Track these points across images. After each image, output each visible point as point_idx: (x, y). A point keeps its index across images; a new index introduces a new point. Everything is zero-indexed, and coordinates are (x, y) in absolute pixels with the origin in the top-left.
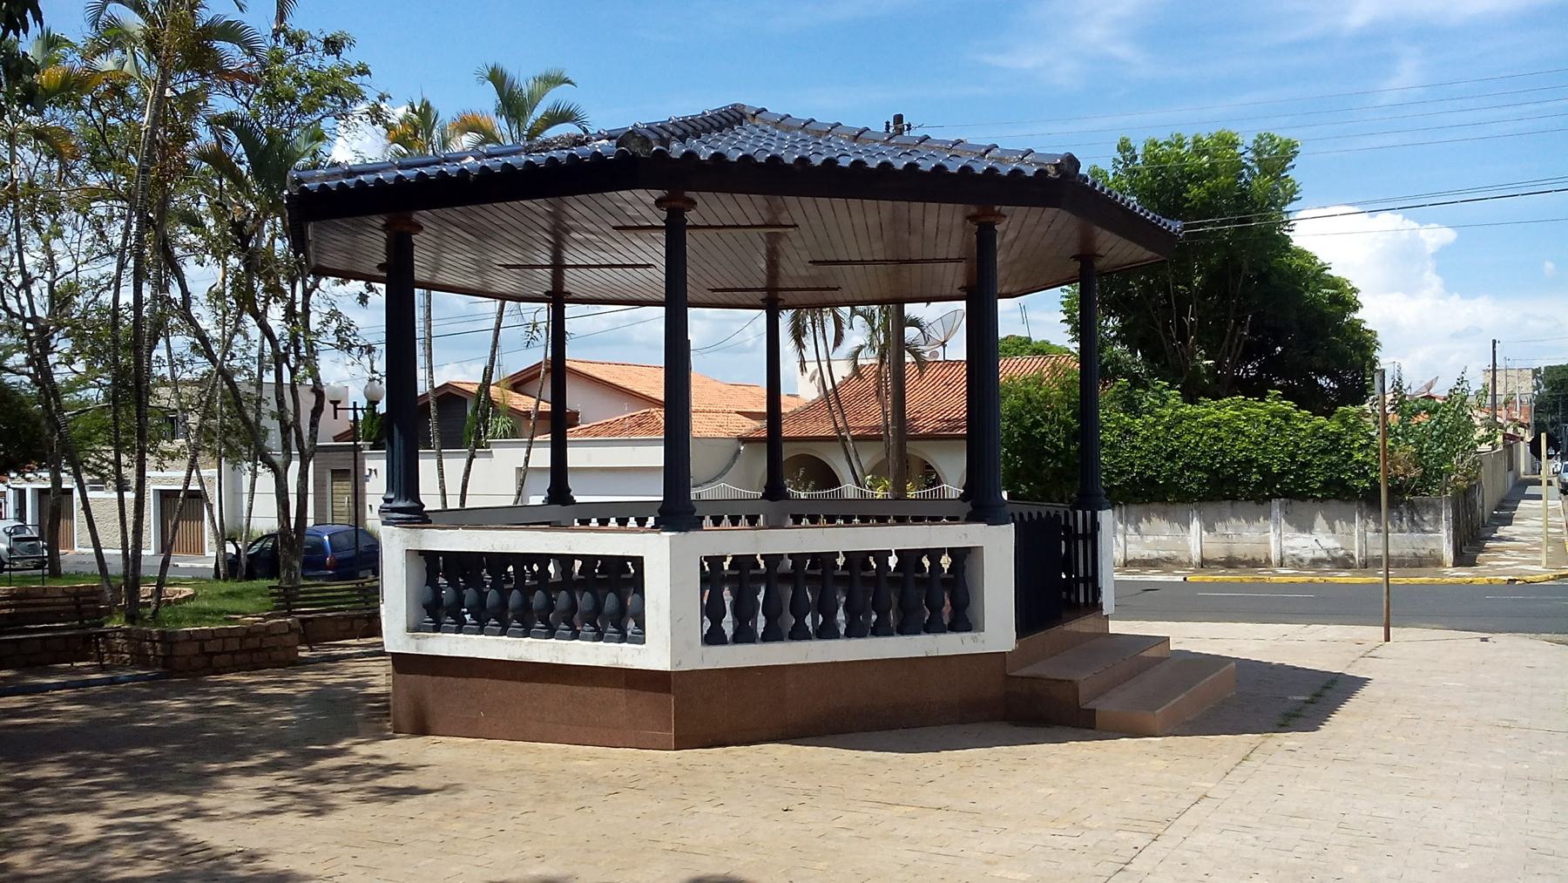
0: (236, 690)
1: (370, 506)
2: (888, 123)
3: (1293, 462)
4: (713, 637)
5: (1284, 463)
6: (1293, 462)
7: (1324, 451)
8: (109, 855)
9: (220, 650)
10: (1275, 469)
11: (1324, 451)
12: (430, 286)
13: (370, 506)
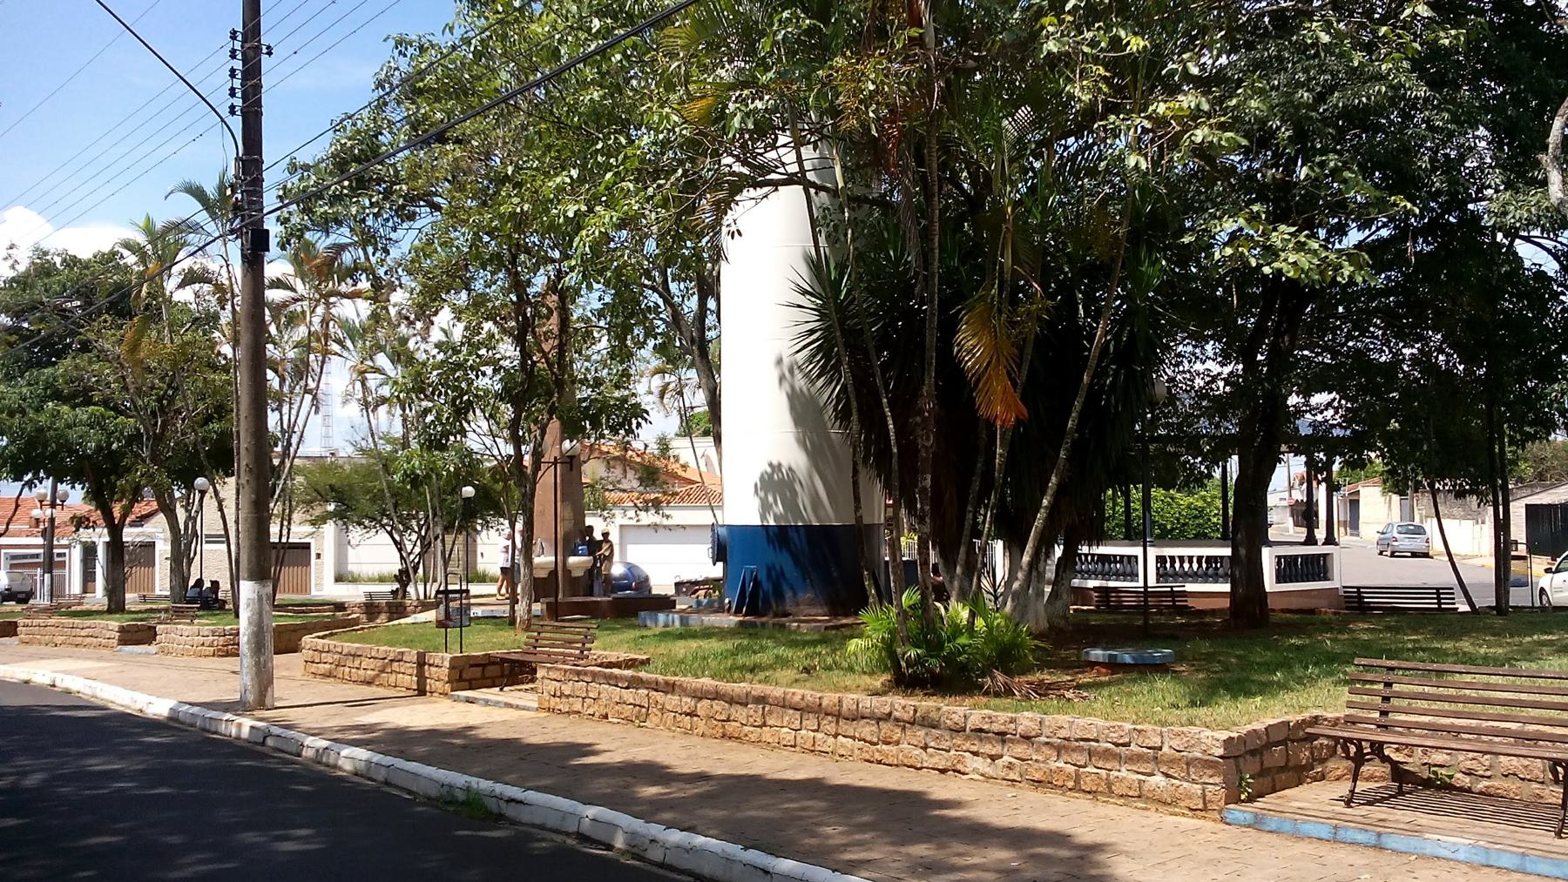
0: (105, 668)
1: (482, 554)
2: (756, 485)
3: (1178, 523)
4: (1158, 582)
5: (1173, 523)
6: (1178, 523)
7: (1196, 517)
8: (39, 777)
9: (1283, 764)
10: (1169, 527)
11: (1196, 517)
12: (430, 665)
13: (482, 554)
